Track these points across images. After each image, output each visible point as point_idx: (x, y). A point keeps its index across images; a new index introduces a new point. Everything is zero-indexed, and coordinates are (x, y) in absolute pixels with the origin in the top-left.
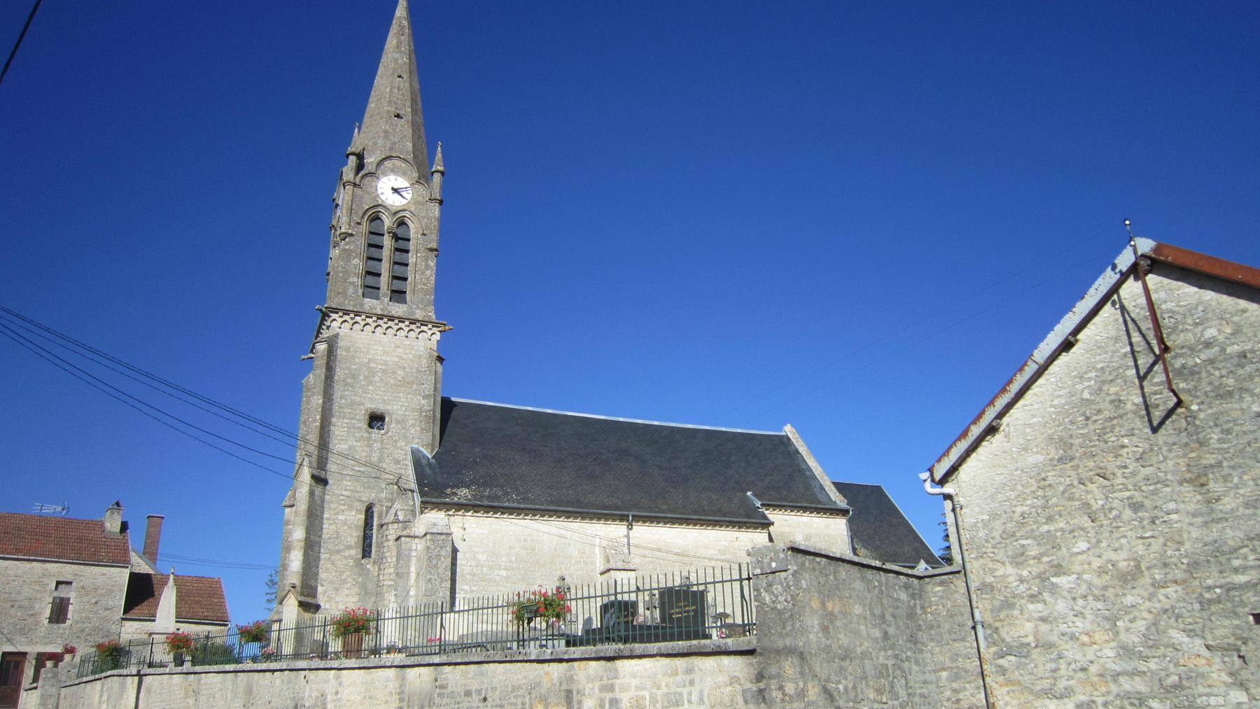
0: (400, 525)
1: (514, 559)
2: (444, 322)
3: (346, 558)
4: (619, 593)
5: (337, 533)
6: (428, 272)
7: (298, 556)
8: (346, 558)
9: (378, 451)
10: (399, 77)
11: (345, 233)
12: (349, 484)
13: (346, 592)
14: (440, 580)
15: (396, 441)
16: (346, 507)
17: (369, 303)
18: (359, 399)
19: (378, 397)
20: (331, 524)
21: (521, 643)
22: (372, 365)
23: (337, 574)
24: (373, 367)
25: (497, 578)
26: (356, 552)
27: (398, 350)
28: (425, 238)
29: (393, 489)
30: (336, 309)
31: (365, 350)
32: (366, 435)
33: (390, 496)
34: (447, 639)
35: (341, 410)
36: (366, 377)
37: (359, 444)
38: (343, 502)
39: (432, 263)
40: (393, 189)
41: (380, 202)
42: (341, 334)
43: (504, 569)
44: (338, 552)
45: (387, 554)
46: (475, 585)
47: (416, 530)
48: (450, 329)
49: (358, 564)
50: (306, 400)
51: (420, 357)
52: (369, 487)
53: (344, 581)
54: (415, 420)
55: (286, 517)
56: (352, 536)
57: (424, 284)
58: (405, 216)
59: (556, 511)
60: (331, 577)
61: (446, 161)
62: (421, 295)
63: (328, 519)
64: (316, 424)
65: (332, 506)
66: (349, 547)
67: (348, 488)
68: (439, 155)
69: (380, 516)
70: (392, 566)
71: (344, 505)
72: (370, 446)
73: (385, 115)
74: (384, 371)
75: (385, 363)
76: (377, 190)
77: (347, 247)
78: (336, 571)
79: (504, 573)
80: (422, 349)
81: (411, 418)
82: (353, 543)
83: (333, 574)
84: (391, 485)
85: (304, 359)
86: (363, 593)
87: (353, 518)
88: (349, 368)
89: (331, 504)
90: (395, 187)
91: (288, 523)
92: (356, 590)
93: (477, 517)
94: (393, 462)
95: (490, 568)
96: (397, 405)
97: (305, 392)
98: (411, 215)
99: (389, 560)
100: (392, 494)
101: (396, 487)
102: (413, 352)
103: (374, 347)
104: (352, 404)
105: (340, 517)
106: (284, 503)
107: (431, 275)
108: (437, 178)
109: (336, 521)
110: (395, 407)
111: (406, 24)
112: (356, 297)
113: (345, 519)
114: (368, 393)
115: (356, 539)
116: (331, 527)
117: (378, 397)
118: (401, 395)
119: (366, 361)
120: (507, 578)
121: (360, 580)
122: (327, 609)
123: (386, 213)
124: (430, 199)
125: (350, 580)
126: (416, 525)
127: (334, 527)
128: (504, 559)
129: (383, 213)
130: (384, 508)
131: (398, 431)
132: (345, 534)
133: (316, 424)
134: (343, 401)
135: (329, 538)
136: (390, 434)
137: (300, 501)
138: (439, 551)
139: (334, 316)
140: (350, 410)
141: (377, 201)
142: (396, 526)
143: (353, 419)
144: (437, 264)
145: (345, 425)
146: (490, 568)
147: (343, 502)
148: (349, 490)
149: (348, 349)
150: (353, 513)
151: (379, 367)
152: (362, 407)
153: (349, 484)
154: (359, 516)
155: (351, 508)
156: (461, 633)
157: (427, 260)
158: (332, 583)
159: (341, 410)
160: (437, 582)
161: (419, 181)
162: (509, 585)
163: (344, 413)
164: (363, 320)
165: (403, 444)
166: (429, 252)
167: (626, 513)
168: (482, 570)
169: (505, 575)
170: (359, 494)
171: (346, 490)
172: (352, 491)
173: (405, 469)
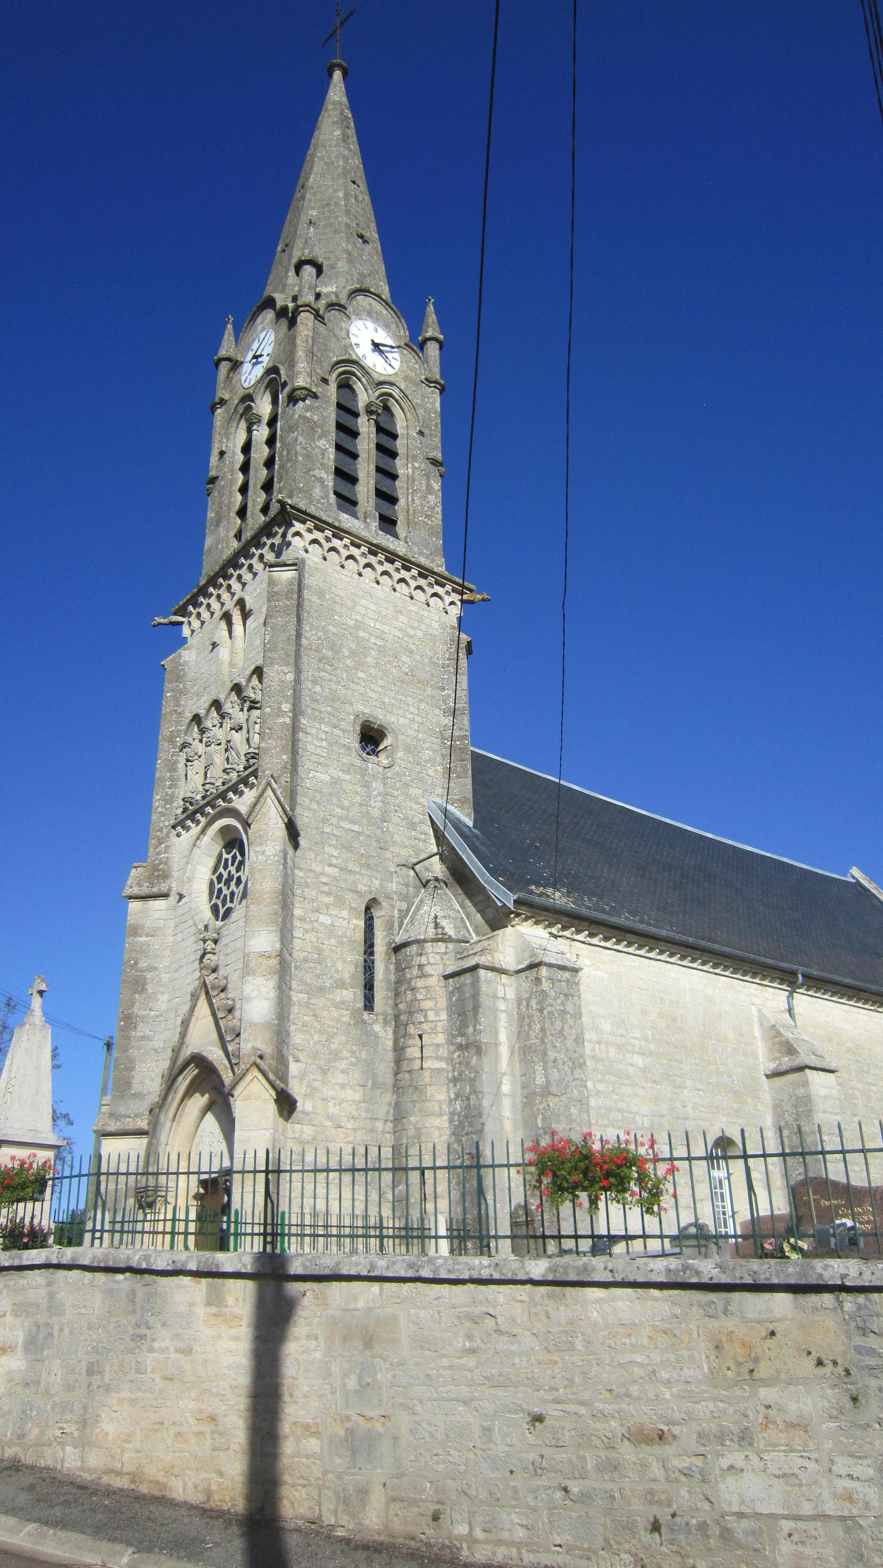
0: (451, 946)
1: (649, 1033)
2: (472, 586)
3: (337, 1006)
4: (104, 1174)
5: (320, 952)
6: (431, 498)
7: (264, 990)
8: (337, 1006)
9: (379, 798)
10: (354, 182)
11: (305, 388)
12: (335, 853)
13: (341, 1078)
14: (570, 1063)
15: (406, 785)
16: (332, 899)
17: (345, 520)
18: (344, 691)
19: (373, 695)
20: (306, 931)
21: (98, 1235)
22: (361, 634)
23: (324, 1037)
24: (364, 639)
25: (631, 1069)
26: (353, 995)
27: (402, 618)
28: (424, 440)
29: (408, 876)
30: (305, 513)
31: (350, 604)
32: (358, 762)
33: (404, 890)
34: (36, 1221)
35: (315, 706)
36: (353, 654)
37: (348, 777)
38: (326, 888)
39: (437, 486)
40: (372, 341)
41: (354, 357)
42: (308, 562)
43: (639, 1053)
44: (322, 990)
45: (426, 1005)
46: (600, 1082)
47: (501, 957)
48: (483, 600)
49: (360, 1023)
50: (174, 697)
51: (433, 638)
52: (368, 866)
53: (335, 1056)
54: (434, 751)
55: (131, 920)
56: (344, 961)
57: (427, 516)
58: (391, 395)
59: (703, 950)
60: (311, 1042)
61: (443, 325)
62: (424, 534)
63: (302, 919)
64: (281, 720)
65: (310, 893)
66: (341, 984)
67: (334, 861)
68: (431, 317)
69: (390, 927)
70: (439, 1029)
71: (329, 894)
72: (367, 785)
73: (343, 228)
74: (380, 650)
75: (381, 636)
76: (348, 336)
77: (308, 414)
78: (320, 1032)
79: (638, 1060)
80: (436, 625)
81: (427, 745)
82: (346, 976)
83: (316, 1037)
84: (404, 868)
85: (160, 624)
86: (370, 1084)
87: (345, 923)
88: (326, 632)
89: (306, 890)
90: (376, 341)
91: (136, 931)
92: (356, 1075)
93: (590, 944)
94: (404, 823)
95: (620, 1047)
96: (404, 716)
97: (171, 682)
98: (401, 395)
99: (431, 1016)
100: (407, 885)
101: (412, 873)
102: (423, 627)
103: (363, 602)
104: (333, 699)
105: (323, 919)
106: (128, 891)
107: (436, 505)
108: (433, 349)
109: (316, 925)
110: (402, 720)
111: (350, 115)
112: (326, 505)
113: (332, 925)
114: (358, 684)
115: (351, 968)
116: (307, 936)
117: (373, 695)
118: (410, 700)
119: (351, 623)
120: (645, 1070)
121: (364, 1055)
122: (308, 1114)
123: (363, 379)
124: (426, 379)
125: (346, 1054)
126: (500, 947)
127: (311, 937)
128: (637, 1034)
129: (359, 379)
130: (396, 912)
131: (409, 766)
132: (332, 954)
133: (281, 720)
134: (318, 689)
135: (305, 960)
136: (396, 768)
137: (260, 871)
138: (563, 1004)
139: (298, 526)
140: (329, 709)
141: (350, 354)
142: (441, 947)
143: (335, 727)
144: (444, 488)
145: (324, 736)
146: (620, 1047)
147: (326, 888)
148: (335, 866)
149: (321, 594)
150: (345, 913)
151: (373, 641)
152: (348, 708)
153: (335, 853)
154: (355, 921)
155: (340, 902)
156: (73, 1206)
157: (428, 479)
158: (315, 1056)
159: (315, 706)
160: (566, 1069)
161: (411, 344)
162: (649, 1084)
163: (321, 712)
164: (346, 546)
165: (418, 792)
166: (431, 466)
167: (795, 967)
168: (608, 1052)
169: (641, 1065)
170: (352, 878)
171: (330, 865)
172: (341, 869)
173: (425, 841)
